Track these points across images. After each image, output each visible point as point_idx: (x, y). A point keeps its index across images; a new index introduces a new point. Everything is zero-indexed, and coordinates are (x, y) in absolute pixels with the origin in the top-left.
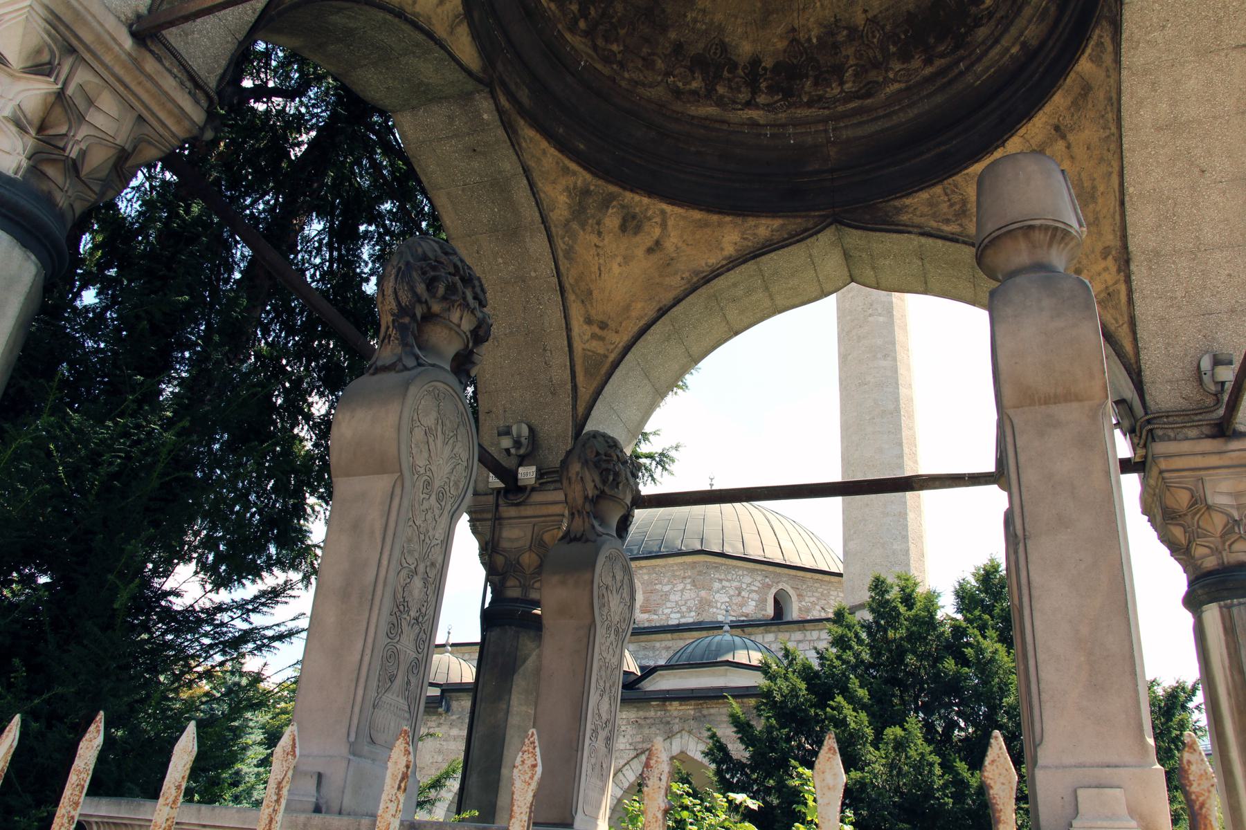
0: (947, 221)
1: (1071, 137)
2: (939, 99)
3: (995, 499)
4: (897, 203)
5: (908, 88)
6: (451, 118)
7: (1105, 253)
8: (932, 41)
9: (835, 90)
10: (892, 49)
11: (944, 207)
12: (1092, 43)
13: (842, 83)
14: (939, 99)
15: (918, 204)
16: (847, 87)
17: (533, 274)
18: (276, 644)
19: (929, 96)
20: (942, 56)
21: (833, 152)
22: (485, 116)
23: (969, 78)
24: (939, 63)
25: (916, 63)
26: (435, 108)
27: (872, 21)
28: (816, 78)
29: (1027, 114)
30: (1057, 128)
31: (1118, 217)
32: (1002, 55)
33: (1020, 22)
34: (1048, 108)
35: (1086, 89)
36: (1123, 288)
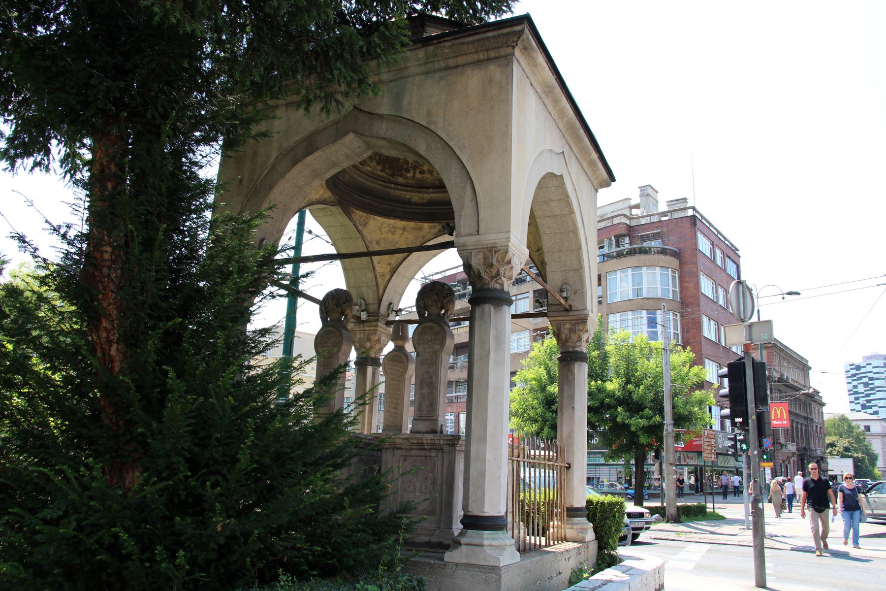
2: (380, 188)
3: (287, 299)
7: (389, 264)
14: (380, 188)
15: (358, 214)
18: (278, 298)
21: (347, 176)
23: (392, 191)
24: (384, 174)
25: (379, 168)
29: (402, 218)
33: (417, 194)
34: (408, 223)
35: (420, 229)
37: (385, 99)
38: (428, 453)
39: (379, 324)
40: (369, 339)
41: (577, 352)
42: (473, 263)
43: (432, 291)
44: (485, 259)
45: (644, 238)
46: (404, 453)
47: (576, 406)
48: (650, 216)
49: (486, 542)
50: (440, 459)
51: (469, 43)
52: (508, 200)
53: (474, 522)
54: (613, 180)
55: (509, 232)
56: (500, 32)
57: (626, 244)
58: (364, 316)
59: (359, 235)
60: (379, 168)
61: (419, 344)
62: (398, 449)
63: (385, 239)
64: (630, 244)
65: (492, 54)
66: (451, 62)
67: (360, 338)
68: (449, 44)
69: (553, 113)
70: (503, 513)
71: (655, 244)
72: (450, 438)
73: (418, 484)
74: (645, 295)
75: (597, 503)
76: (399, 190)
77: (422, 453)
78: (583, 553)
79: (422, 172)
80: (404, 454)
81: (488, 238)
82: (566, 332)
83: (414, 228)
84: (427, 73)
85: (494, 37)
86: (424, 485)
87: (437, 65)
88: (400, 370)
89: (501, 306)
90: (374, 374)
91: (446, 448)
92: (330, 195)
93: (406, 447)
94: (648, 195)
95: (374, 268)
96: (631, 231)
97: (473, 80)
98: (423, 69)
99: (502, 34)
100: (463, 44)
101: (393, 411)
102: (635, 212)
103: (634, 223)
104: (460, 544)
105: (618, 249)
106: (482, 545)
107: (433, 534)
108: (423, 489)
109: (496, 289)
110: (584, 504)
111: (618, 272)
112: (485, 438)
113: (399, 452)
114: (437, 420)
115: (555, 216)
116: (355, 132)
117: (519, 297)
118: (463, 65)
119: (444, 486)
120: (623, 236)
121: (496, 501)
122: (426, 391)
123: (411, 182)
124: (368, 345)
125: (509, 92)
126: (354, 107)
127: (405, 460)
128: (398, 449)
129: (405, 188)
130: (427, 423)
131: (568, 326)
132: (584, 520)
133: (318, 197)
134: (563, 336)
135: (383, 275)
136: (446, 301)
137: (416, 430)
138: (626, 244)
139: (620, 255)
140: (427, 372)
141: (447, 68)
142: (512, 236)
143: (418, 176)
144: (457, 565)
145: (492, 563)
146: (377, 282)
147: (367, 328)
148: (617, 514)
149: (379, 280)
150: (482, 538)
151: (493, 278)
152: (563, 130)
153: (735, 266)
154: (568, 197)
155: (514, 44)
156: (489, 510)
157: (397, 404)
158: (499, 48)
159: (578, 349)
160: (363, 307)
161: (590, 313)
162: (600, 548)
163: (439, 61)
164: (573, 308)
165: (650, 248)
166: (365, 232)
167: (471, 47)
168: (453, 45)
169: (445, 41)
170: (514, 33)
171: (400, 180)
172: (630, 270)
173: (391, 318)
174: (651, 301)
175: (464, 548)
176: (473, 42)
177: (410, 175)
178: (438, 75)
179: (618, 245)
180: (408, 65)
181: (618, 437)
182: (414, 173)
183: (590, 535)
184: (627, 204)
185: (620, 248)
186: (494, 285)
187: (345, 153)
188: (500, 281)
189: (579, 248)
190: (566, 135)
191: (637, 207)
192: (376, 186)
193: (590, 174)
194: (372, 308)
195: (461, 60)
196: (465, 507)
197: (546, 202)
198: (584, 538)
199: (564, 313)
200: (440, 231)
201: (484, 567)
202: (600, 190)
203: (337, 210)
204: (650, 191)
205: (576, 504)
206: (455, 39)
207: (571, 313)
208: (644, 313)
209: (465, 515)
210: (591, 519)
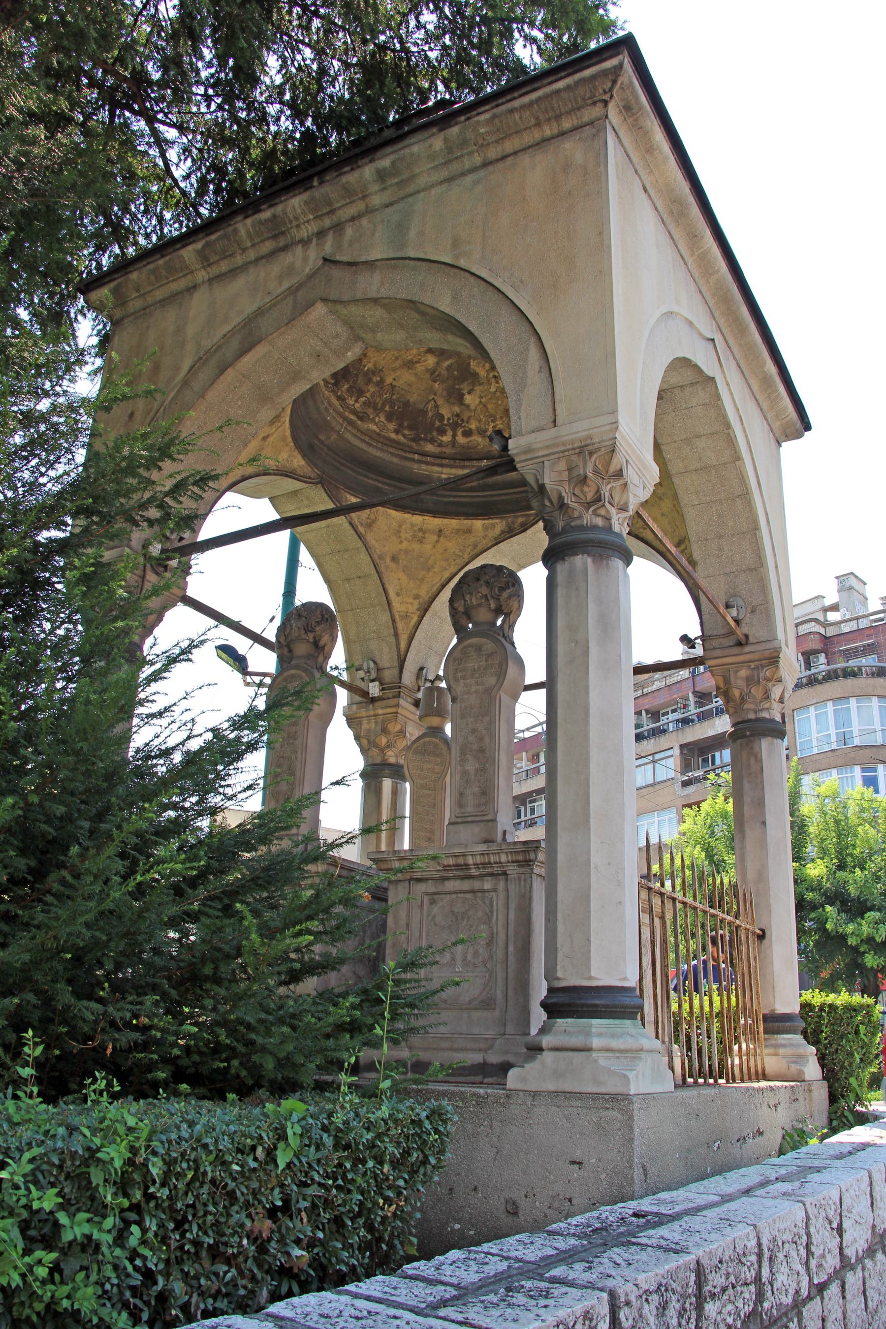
1: (442, 539)
2: (395, 460)
5: (378, 434)
6: (337, 336)
8: (406, 424)
9: (351, 402)
10: (387, 408)
12: (490, 521)
13: (356, 401)
14: (395, 460)
16: (357, 405)
19: (392, 454)
20: (404, 436)
21: (334, 437)
23: (416, 466)
24: (400, 438)
25: (391, 426)
26: (339, 324)
27: (392, 386)
28: (351, 387)
30: (440, 531)
31: (435, 588)
32: (437, 472)
34: (446, 521)
37: (377, 235)
38: (477, 885)
39: (402, 702)
40: (385, 731)
41: (763, 720)
42: (546, 481)
44: (570, 470)
45: (849, 654)
46: (430, 887)
47: (770, 819)
48: (857, 619)
49: (596, 1042)
50: (502, 895)
51: (522, 107)
52: (610, 356)
53: (567, 1003)
54: (807, 427)
55: (614, 412)
56: (577, 76)
57: (821, 664)
58: (374, 690)
59: (360, 544)
60: (391, 426)
61: (456, 680)
62: (419, 880)
63: (406, 552)
64: (828, 663)
65: (567, 124)
66: (493, 153)
67: (369, 731)
68: (487, 116)
69: (690, 262)
70: (632, 981)
71: (869, 661)
72: (519, 848)
74: (857, 742)
75: (822, 1009)
76: (427, 463)
77: (466, 885)
78: (801, 1099)
79: (467, 433)
80: (432, 889)
81: (573, 430)
82: (741, 683)
83: (458, 531)
84: (449, 180)
85: (568, 88)
87: (467, 164)
88: (437, 769)
89: (608, 557)
90: (396, 794)
91: (512, 870)
93: (435, 875)
94: (851, 588)
95: (389, 604)
96: (827, 644)
97: (535, 171)
98: (444, 173)
99: (583, 80)
100: (511, 111)
102: (833, 616)
103: (831, 632)
104: (540, 1049)
105: (808, 673)
106: (590, 1049)
107: (491, 1047)
108: (469, 957)
109: (595, 527)
110: (797, 1009)
111: (812, 709)
112: (587, 821)
113: (421, 888)
114: (494, 820)
115: (705, 468)
116: (324, 300)
117: (657, 757)
118: (515, 153)
119: (511, 948)
120: (816, 652)
121: (615, 957)
123: (448, 451)
124: (384, 741)
125: (602, 194)
126: (325, 260)
127: (433, 902)
128: (419, 880)
129: (438, 461)
131: (743, 673)
132: (799, 1038)
134: (736, 693)
135: (406, 616)
136: (505, 594)
138: (821, 664)
139: (812, 681)
141: (486, 164)
142: (620, 420)
143: (461, 440)
144: (535, 1094)
145: (611, 1087)
146: (395, 629)
147: (380, 711)
148: (862, 1028)
149: (400, 625)
150: (588, 1034)
151: (589, 505)
152: (712, 303)
154: (728, 426)
155: (606, 97)
156: (601, 975)
157: (432, 832)
158: (579, 109)
159: (765, 715)
160: (373, 675)
161: (783, 646)
162: (833, 1098)
163: (471, 153)
164: (751, 640)
165: (860, 669)
166: (370, 538)
167: (526, 114)
168: (495, 117)
169: (478, 114)
170: (605, 73)
171: (430, 448)
172: (830, 704)
174: (866, 751)
175: (548, 1057)
176: (531, 104)
177: (447, 438)
178: (470, 178)
179: (808, 666)
180: (417, 171)
181: (830, 959)
182: (454, 436)
183: (813, 1070)
184: (818, 605)
185: (813, 671)
186: (589, 518)
187: (312, 347)
188: (602, 512)
189: (756, 528)
190: (716, 315)
191: (835, 608)
192: (387, 457)
193: (765, 405)
194: (389, 675)
195: (509, 146)
196: (550, 974)
197: (688, 441)
198: (801, 1072)
199: (736, 650)
200: (502, 532)
201: (595, 1096)
202: (783, 444)
204: (853, 582)
205: (781, 1008)
206: (497, 106)
207: (747, 649)
208: (857, 769)
209: (551, 990)
210: (812, 1037)
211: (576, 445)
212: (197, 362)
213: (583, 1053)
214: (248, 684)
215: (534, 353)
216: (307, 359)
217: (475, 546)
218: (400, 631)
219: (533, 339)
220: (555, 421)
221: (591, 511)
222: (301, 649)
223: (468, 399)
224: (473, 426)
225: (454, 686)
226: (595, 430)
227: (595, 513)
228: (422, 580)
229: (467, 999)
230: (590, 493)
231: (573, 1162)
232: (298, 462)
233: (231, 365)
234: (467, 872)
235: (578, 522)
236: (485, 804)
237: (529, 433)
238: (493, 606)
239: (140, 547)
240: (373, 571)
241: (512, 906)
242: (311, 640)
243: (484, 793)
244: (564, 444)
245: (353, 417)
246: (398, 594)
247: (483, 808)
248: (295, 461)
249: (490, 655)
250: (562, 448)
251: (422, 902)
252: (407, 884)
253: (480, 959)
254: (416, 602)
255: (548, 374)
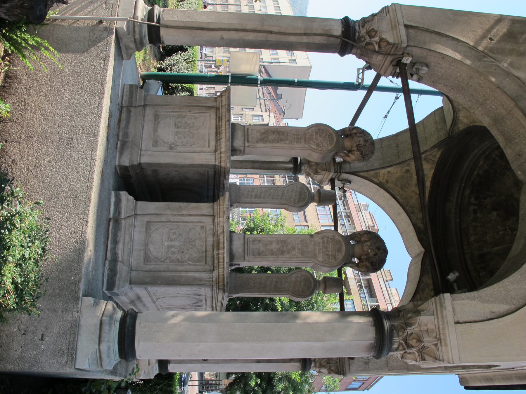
0: (426, 156)
4: (442, 150)
7: (387, 181)
11: (431, 157)
16: (494, 156)
17: (480, 109)
22: (520, 173)
31: (391, 191)
36: (376, 181)
43: (378, 249)
46: (210, 227)
61: (323, 237)
73: (177, 243)
77: (210, 248)
79: (475, 212)
86: (176, 250)
88: (292, 200)
92: (461, 129)
95: (384, 168)
101: (254, 194)
108: (172, 249)
122: (274, 246)
127: (202, 227)
130: (240, 250)
133: (461, 118)
135: (377, 176)
137: (235, 237)
140: (294, 248)
149: (372, 173)
151: (406, 340)
153: (357, 387)
173: (337, 182)
177: (473, 200)
203: (443, 135)
211: (442, 336)
212: (522, 81)
213: (97, 341)
214: (359, 70)
215: (504, 308)
216: (518, 148)
217: (413, 213)
218: (369, 173)
219: (513, 307)
220: (458, 323)
221: (401, 341)
222: (348, 143)
223: (495, 214)
224: (479, 215)
225: (319, 236)
226: (449, 349)
227: (400, 344)
228: (396, 185)
229: (151, 248)
230: (413, 342)
231: (43, 335)
232: (461, 127)
233: (517, 105)
234: (215, 249)
235: (395, 335)
236: (253, 255)
237: (452, 305)
238: (363, 257)
239: (407, 52)
240: (401, 161)
241: (196, 275)
242: (353, 149)
243: (259, 254)
244: (443, 329)
245: (487, 153)
246: (388, 172)
247: (251, 253)
248: (462, 125)
249: (334, 257)
250: (441, 327)
251: (203, 222)
252: (212, 214)
253: (171, 255)
254: (384, 181)
255: (489, 317)
